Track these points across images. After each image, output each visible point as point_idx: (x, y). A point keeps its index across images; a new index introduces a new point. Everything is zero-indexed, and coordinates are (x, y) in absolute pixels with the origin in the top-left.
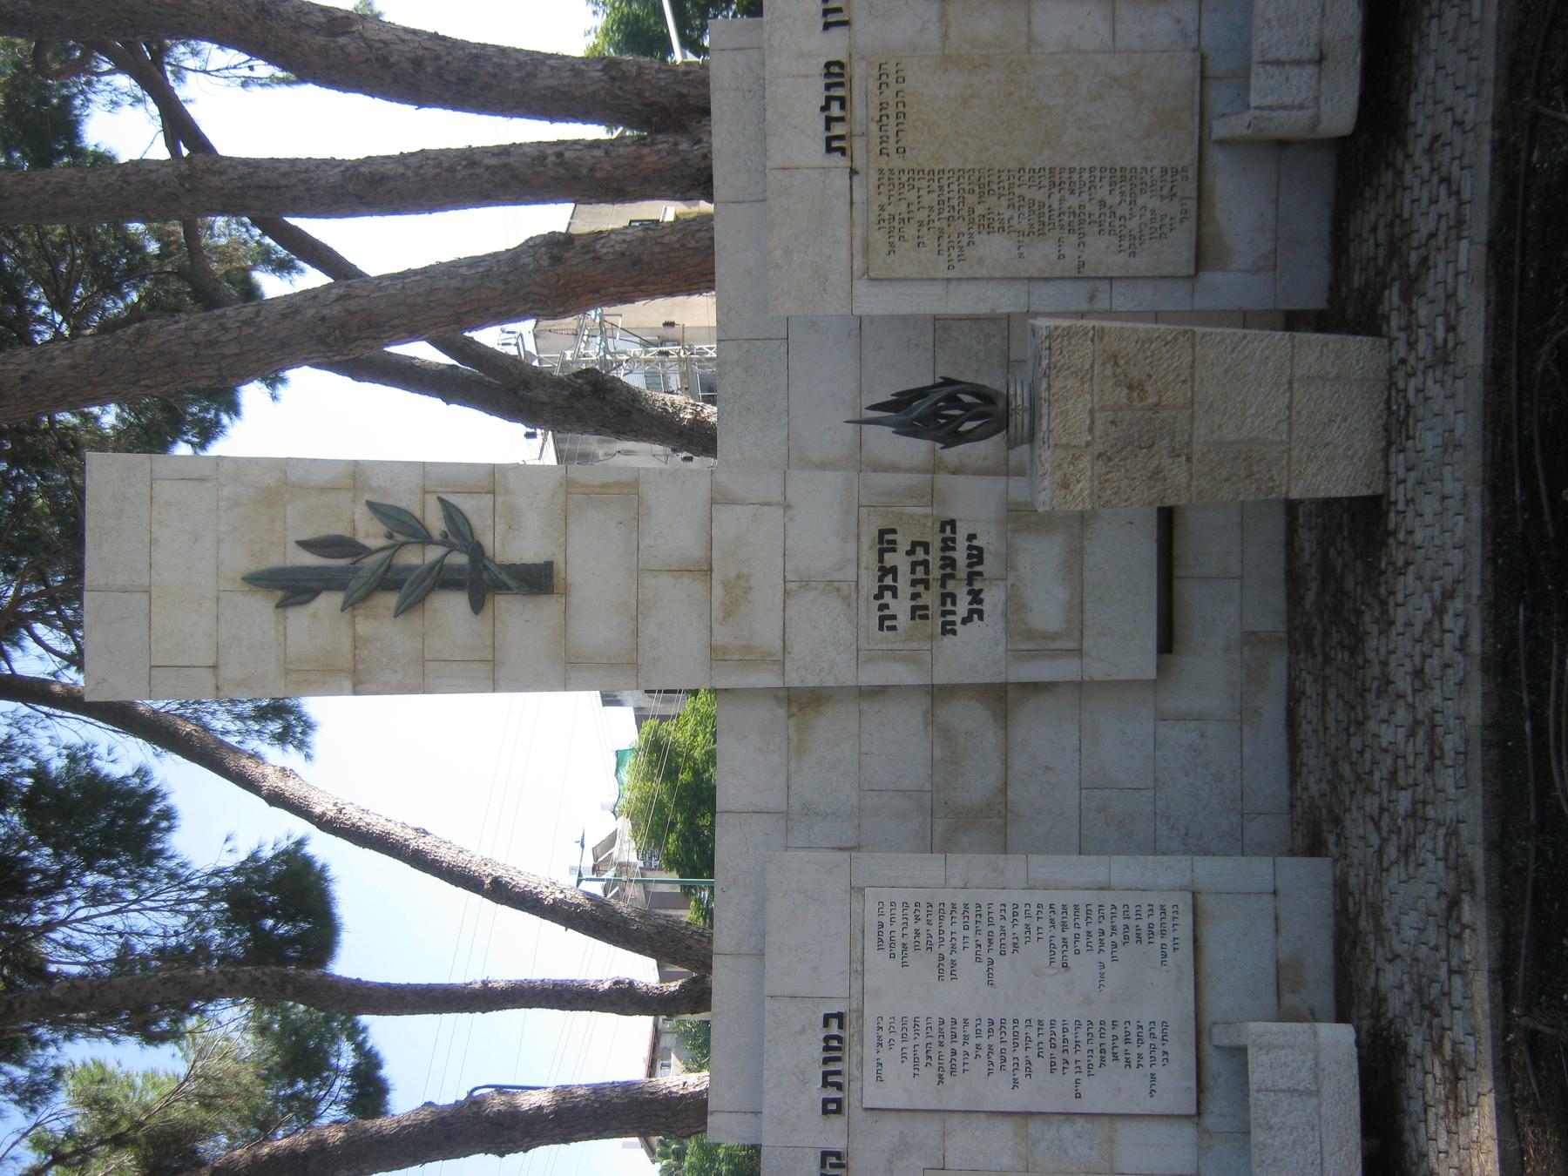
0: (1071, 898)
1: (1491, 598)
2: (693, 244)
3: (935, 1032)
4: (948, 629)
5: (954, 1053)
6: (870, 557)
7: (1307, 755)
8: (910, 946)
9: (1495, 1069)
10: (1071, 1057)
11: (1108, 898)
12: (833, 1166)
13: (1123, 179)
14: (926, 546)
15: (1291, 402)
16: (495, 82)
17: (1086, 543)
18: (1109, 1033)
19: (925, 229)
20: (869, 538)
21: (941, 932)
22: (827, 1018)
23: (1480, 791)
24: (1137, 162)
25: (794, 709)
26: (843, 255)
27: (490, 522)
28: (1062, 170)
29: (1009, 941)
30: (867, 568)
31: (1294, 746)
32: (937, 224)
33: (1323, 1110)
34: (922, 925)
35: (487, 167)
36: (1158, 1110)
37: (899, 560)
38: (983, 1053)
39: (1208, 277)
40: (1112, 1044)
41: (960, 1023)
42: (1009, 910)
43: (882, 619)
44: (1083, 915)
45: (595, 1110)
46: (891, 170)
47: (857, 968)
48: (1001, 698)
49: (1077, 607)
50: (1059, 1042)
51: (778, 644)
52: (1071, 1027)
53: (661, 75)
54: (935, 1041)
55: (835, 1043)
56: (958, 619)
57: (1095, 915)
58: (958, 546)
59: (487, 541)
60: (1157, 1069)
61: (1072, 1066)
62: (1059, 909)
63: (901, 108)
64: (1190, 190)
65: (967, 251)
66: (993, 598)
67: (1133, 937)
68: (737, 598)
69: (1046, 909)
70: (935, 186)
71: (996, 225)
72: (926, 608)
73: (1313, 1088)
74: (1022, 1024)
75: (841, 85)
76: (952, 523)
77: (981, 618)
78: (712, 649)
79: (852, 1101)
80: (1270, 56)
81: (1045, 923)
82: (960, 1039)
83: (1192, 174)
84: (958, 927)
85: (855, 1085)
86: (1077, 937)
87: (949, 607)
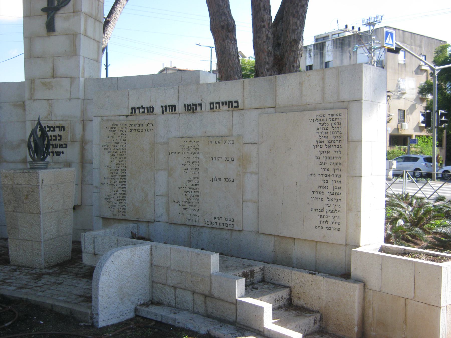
2: (229, 70)
6: (57, 124)
13: (123, 197)
14: (60, 140)
15: (27, 240)
16: (292, 4)
19: (112, 138)
24: (127, 201)
26: (107, 114)
27: (66, 12)
28: (125, 179)
32: (113, 142)
35: (260, 4)
39: (101, 221)
46: (126, 128)
51: (36, 98)
53: (292, 58)
58: (61, 149)
59: (61, 11)
63: (141, 130)
64: (120, 217)
65: (106, 151)
68: (47, 86)
70: (122, 141)
71: (112, 159)
75: (148, 112)
76: (66, 147)
78: (34, 79)
80: (95, 240)
83: (124, 218)
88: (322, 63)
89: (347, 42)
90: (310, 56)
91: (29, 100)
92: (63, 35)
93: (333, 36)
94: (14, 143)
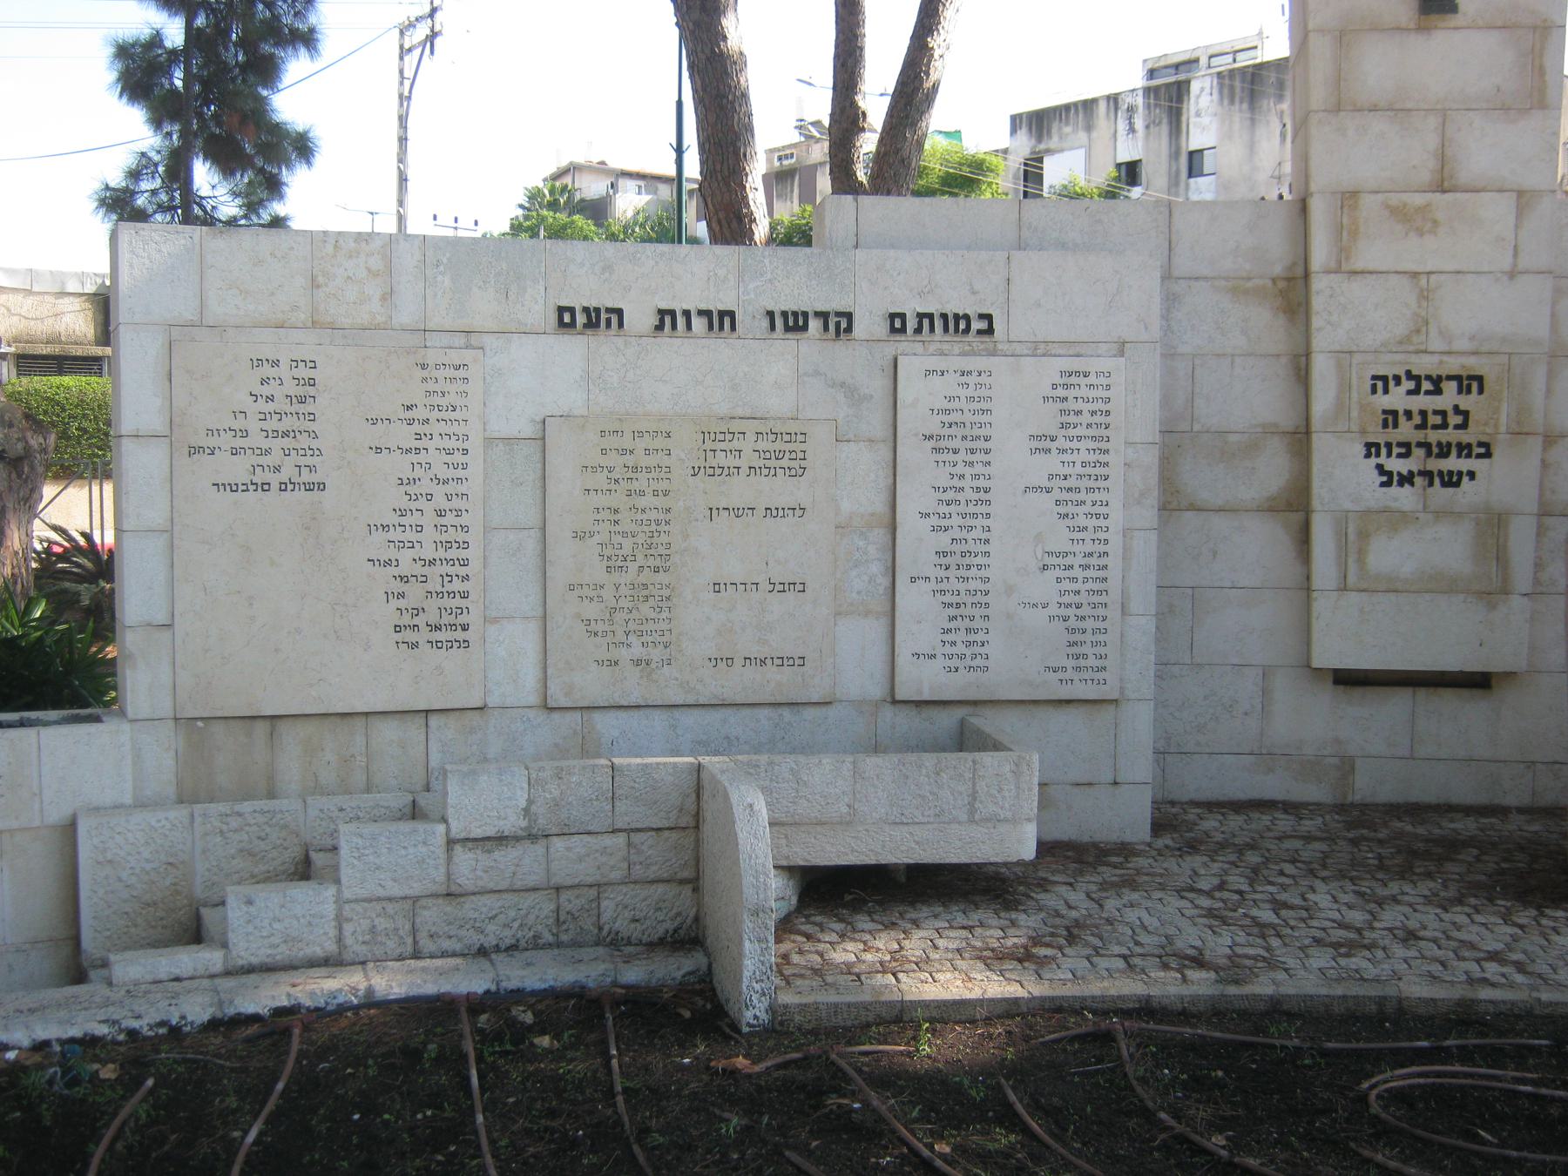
0: (1114, 574)
1: (1537, 1012)
3: (976, 432)
4: (1371, 449)
5: (955, 452)
6: (1453, 365)
7: (1235, 821)
8: (1065, 406)
9: (1052, 999)
10: (952, 573)
11: (1113, 613)
12: (838, 325)
14: (1463, 426)
17: (1462, 597)
18: (977, 612)
20: (1475, 365)
21: (1079, 438)
22: (988, 318)
23: (1332, 993)
25: (1281, 284)
29: (1070, 509)
30: (1441, 362)
31: (1238, 806)
33: (954, 826)
34: (1086, 418)
36: (900, 661)
37: (1449, 397)
38: (956, 482)
40: (965, 614)
41: (986, 458)
42: (1103, 510)
43: (1384, 379)
44: (1096, 586)
45: (725, 96)
47: (1040, 349)
48: (1295, 506)
49: (1392, 586)
50: (967, 560)
51: (1359, 265)
52: (983, 573)
54: (967, 432)
55: (962, 326)
56: (1382, 460)
57: (1096, 599)
58: (1461, 460)
60: (940, 662)
61: (943, 573)
62: (1103, 561)
66: (1404, 497)
67: (1073, 638)
69: (1102, 548)
72: (1396, 425)
73: (977, 817)
74: (986, 522)
76: (1488, 455)
77: (1383, 484)
78: (1354, 194)
79: (904, 344)
81: (1089, 547)
82: (970, 458)
84: (1084, 456)
85: (919, 347)
86: (1074, 580)
87: (1396, 450)
88: (1175, 154)
89: (1272, 77)
90: (1132, 130)
91: (1329, 272)
92: (1491, 27)
93: (1214, 61)
94: (1232, 438)
